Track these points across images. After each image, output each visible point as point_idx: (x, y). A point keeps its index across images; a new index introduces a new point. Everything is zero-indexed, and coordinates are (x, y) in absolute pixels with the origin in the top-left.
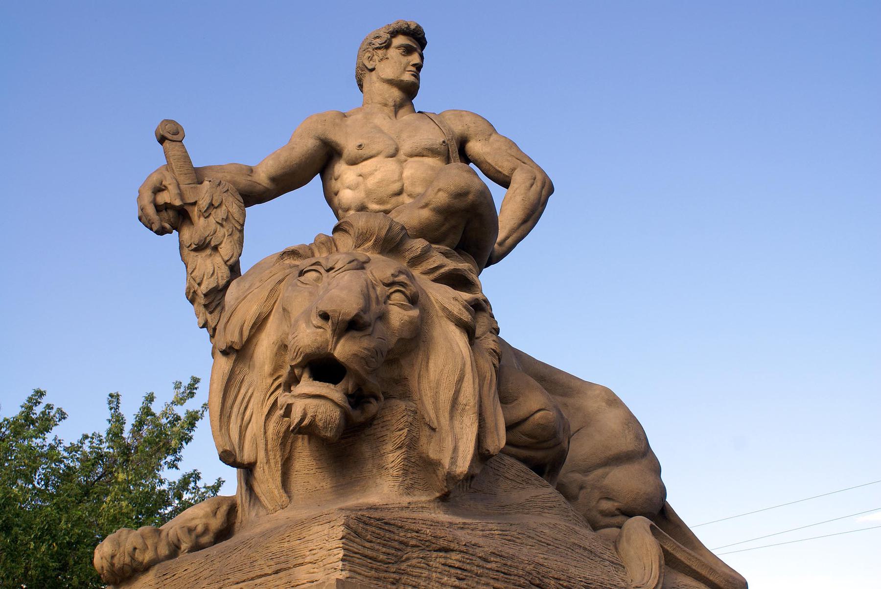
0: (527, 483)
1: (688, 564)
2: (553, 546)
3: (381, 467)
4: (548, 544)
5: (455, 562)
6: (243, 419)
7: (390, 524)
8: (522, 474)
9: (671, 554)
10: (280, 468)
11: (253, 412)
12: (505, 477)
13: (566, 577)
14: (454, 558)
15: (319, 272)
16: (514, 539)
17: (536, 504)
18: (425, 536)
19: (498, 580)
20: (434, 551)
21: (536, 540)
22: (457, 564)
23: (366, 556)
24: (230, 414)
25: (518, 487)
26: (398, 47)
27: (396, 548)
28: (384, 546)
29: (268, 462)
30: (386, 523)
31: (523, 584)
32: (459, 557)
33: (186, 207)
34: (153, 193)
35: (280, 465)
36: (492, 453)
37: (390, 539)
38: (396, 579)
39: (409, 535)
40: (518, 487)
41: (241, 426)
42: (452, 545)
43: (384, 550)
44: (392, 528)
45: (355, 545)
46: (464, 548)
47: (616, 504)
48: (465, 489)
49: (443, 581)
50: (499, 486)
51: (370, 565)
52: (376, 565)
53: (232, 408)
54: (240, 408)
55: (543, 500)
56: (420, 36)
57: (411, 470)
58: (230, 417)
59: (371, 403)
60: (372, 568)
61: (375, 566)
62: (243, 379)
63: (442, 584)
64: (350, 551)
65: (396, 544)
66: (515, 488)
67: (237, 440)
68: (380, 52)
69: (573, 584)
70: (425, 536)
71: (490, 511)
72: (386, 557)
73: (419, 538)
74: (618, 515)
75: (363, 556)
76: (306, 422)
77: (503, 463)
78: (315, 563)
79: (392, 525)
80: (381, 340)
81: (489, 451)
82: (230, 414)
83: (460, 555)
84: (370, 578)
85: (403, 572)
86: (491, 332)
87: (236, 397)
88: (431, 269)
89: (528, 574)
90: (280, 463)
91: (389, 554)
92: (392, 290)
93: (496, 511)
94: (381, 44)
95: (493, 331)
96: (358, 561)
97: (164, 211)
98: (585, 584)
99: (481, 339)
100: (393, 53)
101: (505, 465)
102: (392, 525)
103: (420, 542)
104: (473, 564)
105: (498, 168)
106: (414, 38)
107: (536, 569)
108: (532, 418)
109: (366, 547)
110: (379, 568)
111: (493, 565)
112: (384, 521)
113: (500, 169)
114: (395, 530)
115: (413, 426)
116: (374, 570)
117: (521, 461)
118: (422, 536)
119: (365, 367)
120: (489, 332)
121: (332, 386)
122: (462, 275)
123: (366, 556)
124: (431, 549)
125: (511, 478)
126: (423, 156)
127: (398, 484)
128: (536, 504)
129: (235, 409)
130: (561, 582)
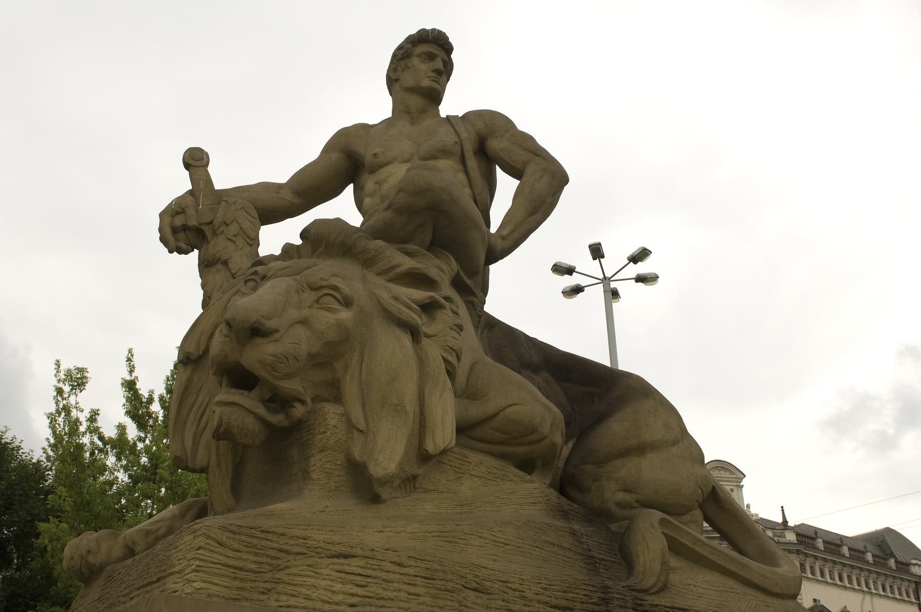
0: (502, 480)
1: (712, 558)
2: (513, 545)
3: (306, 475)
4: (506, 544)
5: (355, 568)
6: (198, 426)
7: (268, 532)
8: (495, 471)
9: (690, 548)
10: (231, 472)
11: (209, 419)
12: (471, 474)
13: (517, 579)
14: (354, 565)
15: (256, 281)
16: (457, 540)
17: (510, 501)
18: (315, 543)
19: (415, 585)
20: (328, 558)
21: (489, 540)
22: (360, 571)
23: (229, 566)
24: (186, 421)
25: (489, 484)
26: (419, 56)
27: (272, 557)
28: (256, 554)
29: (219, 465)
30: (263, 531)
31: (452, 589)
32: (361, 563)
33: (203, 227)
34: (171, 216)
35: (231, 469)
36: (431, 453)
37: (265, 548)
38: (268, 589)
39: (293, 542)
40: (489, 484)
41: (195, 433)
42: (354, 551)
43: (255, 559)
44: (270, 536)
45: (216, 556)
46: (369, 554)
47: (634, 496)
48: (408, 490)
49: (334, 589)
50: (462, 484)
51: (232, 575)
52: (242, 574)
53: (188, 415)
54: (196, 415)
55: (522, 497)
56: (442, 42)
57: (336, 472)
58: (185, 424)
59: (294, 407)
60: (236, 578)
61: (240, 576)
62: (202, 387)
63: (334, 592)
64: (207, 562)
65: (273, 553)
66: (486, 485)
67: (190, 446)
68: (402, 63)
69: (526, 587)
70: (315, 543)
71: (442, 511)
72: (256, 566)
73: (307, 545)
74: (637, 507)
75: (226, 566)
76: (222, 429)
77: (467, 460)
78: (180, 573)
79: (270, 533)
80: (294, 345)
81: (427, 451)
82: (186, 421)
83: (364, 561)
84: (232, 588)
85: (278, 581)
86: (451, 329)
87: (193, 405)
88: (386, 269)
89: (460, 578)
90: (231, 467)
91: (261, 563)
92: (320, 294)
93: (451, 511)
94: (403, 54)
95: (455, 327)
96: (216, 571)
97: (183, 232)
98: (545, 586)
99: (438, 336)
100: (416, 61)
101: (470, 463)
102: (270, 533)
103: (308, 549)
104: (381, 569)
105: (511, 163)
106: (437, 45)
107: (473, 572)
108: (501, 413)
109: (230, 557)
110: (245, 578)
111: (411, 571)
112: (261, 529)
113: (513, 164)
114: (275, 538)
115: (339, 428)
116: (238, 580)
117: (497, 457)
118: (310, 542)
119: (272, 373)
120: (448, 329)
121: (246, 393)
122: (421, 274)
123: (229, 566)
124: (323, 555)
125: (478, 475)
126: (436, 158)
127: (318, 487)
128: (510, 501)
129: (191, 417)
130: (509, 585)
